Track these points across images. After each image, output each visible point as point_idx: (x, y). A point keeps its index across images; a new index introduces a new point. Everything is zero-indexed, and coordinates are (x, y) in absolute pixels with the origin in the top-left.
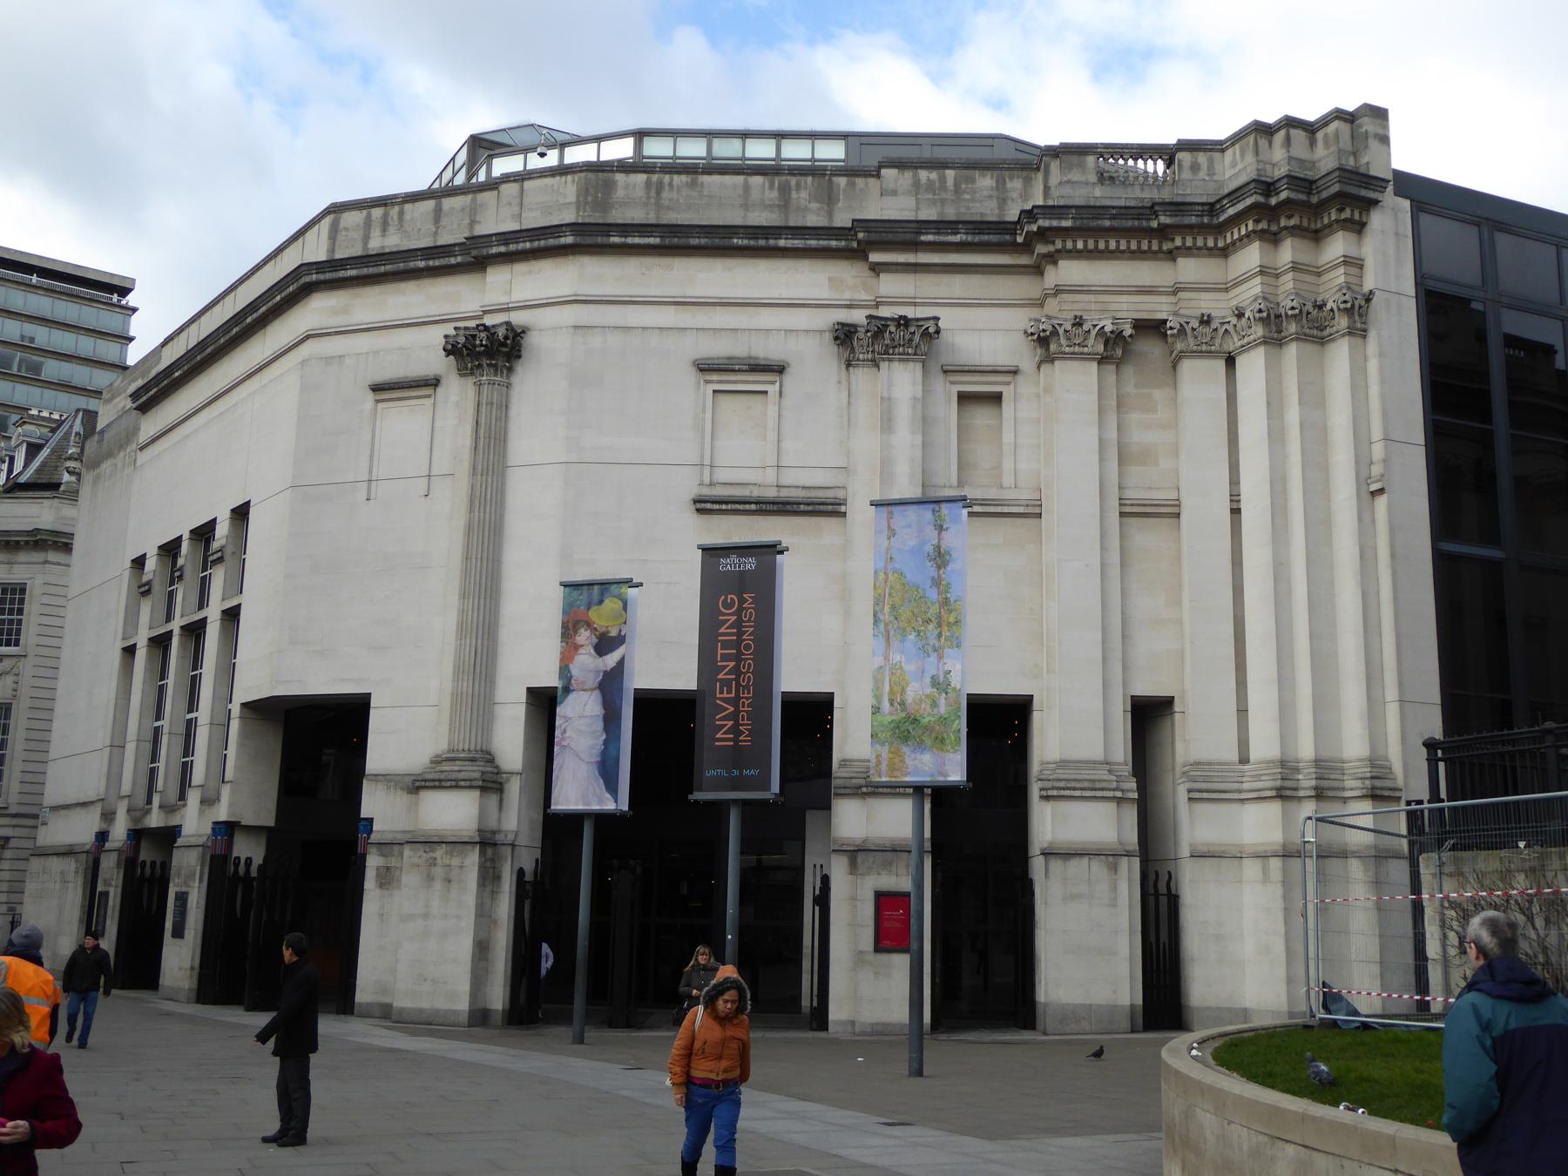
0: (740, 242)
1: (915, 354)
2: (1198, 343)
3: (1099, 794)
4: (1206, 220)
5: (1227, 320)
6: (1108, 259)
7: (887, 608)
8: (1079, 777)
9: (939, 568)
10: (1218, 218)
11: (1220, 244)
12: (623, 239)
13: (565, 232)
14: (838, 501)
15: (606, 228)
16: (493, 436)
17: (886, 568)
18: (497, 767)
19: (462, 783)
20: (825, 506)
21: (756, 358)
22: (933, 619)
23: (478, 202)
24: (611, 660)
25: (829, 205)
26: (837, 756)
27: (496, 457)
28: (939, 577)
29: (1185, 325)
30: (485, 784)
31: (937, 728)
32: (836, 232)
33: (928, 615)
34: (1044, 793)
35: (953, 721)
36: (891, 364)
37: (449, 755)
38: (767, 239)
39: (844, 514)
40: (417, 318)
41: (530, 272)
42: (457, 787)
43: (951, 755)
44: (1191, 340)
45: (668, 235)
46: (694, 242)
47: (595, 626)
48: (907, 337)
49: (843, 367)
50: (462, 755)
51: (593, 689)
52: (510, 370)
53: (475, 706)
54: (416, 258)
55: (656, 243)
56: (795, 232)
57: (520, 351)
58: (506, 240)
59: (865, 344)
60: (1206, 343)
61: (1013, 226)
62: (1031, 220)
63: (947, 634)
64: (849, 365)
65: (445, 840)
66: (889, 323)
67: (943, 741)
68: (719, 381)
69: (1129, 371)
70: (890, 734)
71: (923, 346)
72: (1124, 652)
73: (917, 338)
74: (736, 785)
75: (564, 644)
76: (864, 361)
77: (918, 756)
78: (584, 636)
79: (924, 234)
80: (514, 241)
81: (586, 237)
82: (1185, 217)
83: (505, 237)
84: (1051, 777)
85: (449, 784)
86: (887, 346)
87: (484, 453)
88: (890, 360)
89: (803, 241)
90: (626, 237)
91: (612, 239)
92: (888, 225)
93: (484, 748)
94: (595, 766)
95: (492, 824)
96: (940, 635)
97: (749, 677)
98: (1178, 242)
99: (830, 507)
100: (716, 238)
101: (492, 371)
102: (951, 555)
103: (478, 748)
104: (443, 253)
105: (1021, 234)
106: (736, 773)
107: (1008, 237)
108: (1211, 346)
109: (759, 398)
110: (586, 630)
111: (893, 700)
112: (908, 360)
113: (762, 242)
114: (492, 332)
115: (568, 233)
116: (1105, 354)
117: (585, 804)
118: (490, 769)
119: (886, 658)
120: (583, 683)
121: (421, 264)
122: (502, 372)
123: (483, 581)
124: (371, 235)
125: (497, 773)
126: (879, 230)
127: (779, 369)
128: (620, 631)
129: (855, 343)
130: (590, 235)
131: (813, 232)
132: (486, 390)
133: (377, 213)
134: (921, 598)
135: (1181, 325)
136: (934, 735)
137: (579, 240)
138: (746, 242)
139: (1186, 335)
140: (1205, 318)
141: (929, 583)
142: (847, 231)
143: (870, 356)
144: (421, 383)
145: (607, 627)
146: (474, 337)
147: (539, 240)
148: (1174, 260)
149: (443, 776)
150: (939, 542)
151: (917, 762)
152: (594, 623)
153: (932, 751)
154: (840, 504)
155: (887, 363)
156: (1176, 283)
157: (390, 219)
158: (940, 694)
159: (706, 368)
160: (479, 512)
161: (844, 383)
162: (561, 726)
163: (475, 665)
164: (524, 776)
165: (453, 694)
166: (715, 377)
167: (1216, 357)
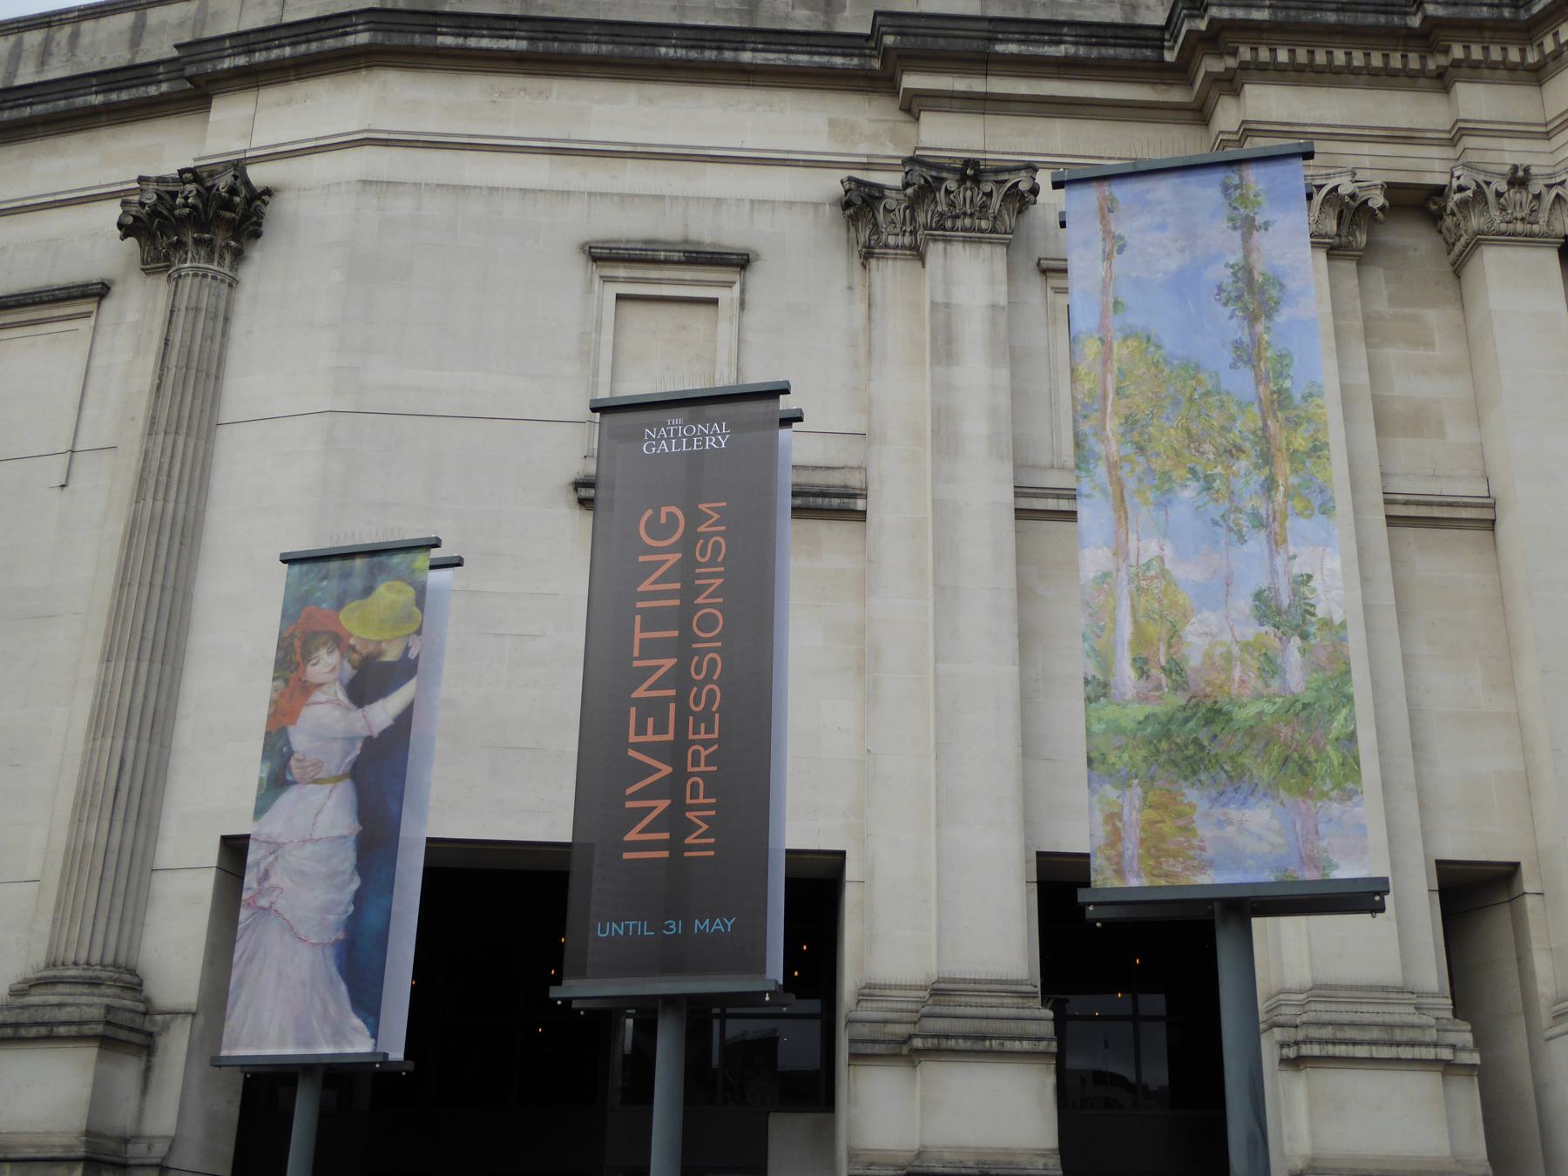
0: (671, 52)
1: (994, 231)
2: (1508, 218)
3: (1406, 1053)
4: (1507, 13)
5: (1558, 180)
6: (1331, 85)
7: (1112, 425)
8: (1357, 1018)
9: (1252, 319)
10: (1529, 9)
11: (1533, 57)
12: (460, 41)
13: (357, 25)
14: (851, 491)
15: (432, 20)
16: (194, 364)
17: (1103, 327)
18: (147, 1001)
19: (62, 1030)
20: (827, 500)
21: (698, 243)
22: (1247, 446)
23: (211, 11)
24: (383, 713)
25: (827, 13)
26: (850, 981)
27: (198, 403)
28: (1256, 341)
29: (1484, 186)
30: (111, 1032)
31: (1285, 731)
32: (843, 41)
33: (1231, 436)
34: (1291, 1053)
35: (1332, 711)
36: (949, 247)
37: (45, 974)
38: (719, 49)
39: (861, 516)
40: (79, 190)
41: (289, 101)
42: (51, 1038)
43: (1335, 809)
44: (1495, 213)
45: (541, 35)
46: (589, 49)
47: (352, 641)
48: (978, 200)
49: (857, 261)
50: (72, 972)
51: (339, 779)
52: (238, 256)
53: (110, 874)
54: (87, 90)
55: (519, 48)
56: (772, 38)
57: (260, 225)
58: (248, 45)
59: (898, 217)
60: (1523, 219)
61: (1157, 34)
62: (1196, 12)
63: (1293, 480)
64: (868, 254)
65: (11, 1156)
66: (945, 175)
67: (1305, 768)
68: (629, 280)
69: (1377, 276)
70: (1143, 752)
71: (1006, 217)
72: (1418, 775)
73: (996, 202)
74: (673, 958)
75: (280, 683)
76: (896, 247)
77: (1233, 812)
78: (326, 666)
79: (1001, 41)
80: (262, 46)
81: (394, 34)
82: (1469, 8)
83: (246, 40)
84: (1298, 1021)
85: (33, 1032)
86: (941, 215)
87: (173, 393)
88: (947, 240)
89: (783, 56)
90: (466, 36)
91: (441, 40)
92: (937, 23)
93: (122, 960)
94: (330, 952)
95: (122, 1118)
96: (1269, 486)
97: (711, 693)
98: (1458, 52)
99: (836, 502)
100: (630, 44)
101: (203, 253)
102: (1282, 286)
103: (109, 959)
104: (135, 78)
105: (1172, 48)
106: (675, 927)
107: (1148, 53)
108: (1532, 224)
109: (702, 312)
110: (329, 653)
111: (1146, 661)
112: (980, 241)
113: (710, 55)
114: (209, 184)
115: (360, 27)
116: (1337, 240)
117: (298, 1044)
118: (127, 1003)
119: (1120, 551)
120: (318, 765)
121: (97, 100)
122: (222, 257)
123: (151, 627)
124: (18, 73)
125: (145, 1014)
126: (921, 31)
127: (741, 262)
128: (407, 649)
129: (881, 217)
130: (400, 31)
131: (802, 40)
132: (187, 290)
133: (34, 38)
134: (1208, 393)
135: (1478, 185)
136: (1276, 751)
137: (380, 38)
138: (681, 53)
139: (1486, 203)
140: (1521, 173)
141: (1227, 356)
142: (862, 42)
143: (907, 240)
144: (75, 292)
145: (379, 642)
146: (174, 195)
147: (308, 41)
148: (1446, 89)
149: (24, 1017)
150: (1246, 256)
151: (1230, 830)
152: (351, 635)
153: (1274, 798)
154: (854, 496)
155: (941, 245)
156: (1457, 121)
157: (54, 45)
158: (1284, 638)
159: (602, 255)
160: (154, 499)
161: (859, 291)
162: (258, 864)
163: (117, 790)
164: (200, 1020)
165: (67, 849)
166: (621, 272)
167: (1540, 245)
